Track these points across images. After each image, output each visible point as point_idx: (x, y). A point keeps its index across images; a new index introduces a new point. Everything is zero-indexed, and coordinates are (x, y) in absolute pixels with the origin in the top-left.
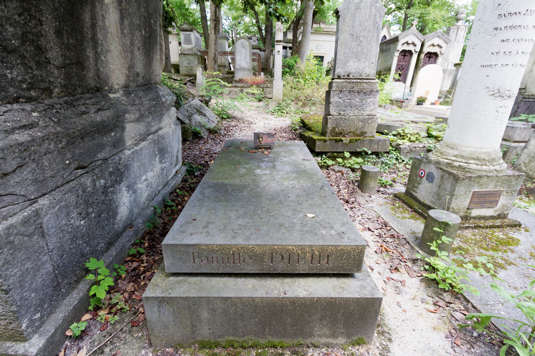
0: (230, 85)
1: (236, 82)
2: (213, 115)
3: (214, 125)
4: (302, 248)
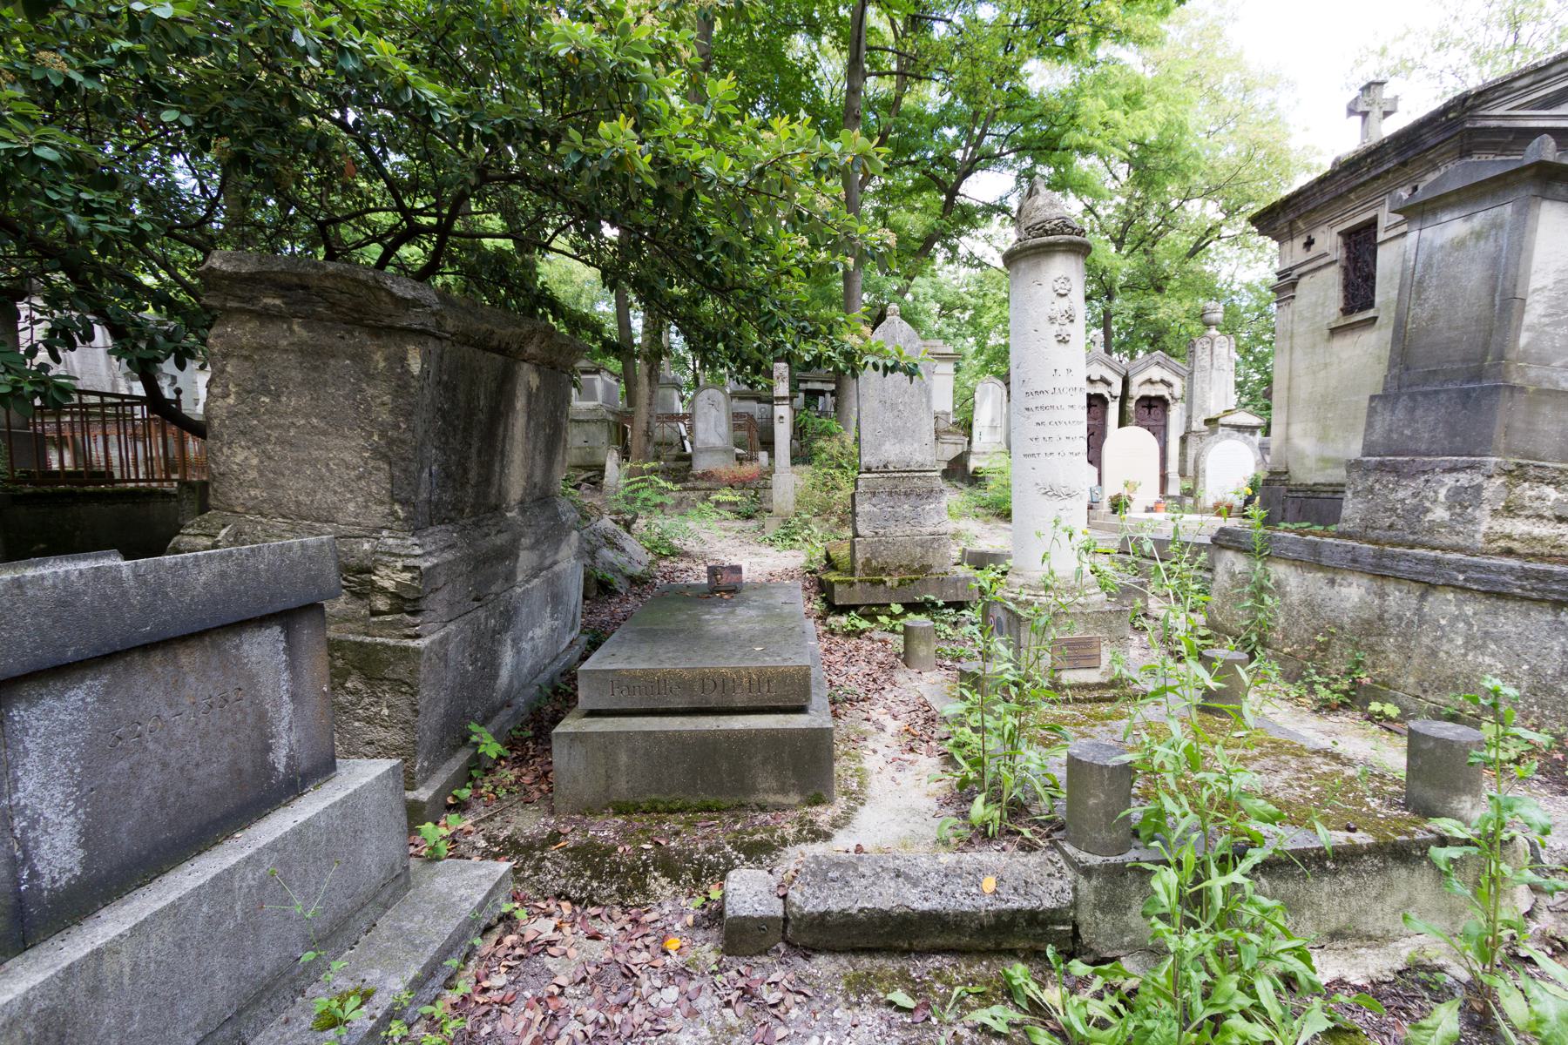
0: (678, 486)
1: (696, 478)
2: (639, 548)
3: (641, 568)
4: (737, 671)
